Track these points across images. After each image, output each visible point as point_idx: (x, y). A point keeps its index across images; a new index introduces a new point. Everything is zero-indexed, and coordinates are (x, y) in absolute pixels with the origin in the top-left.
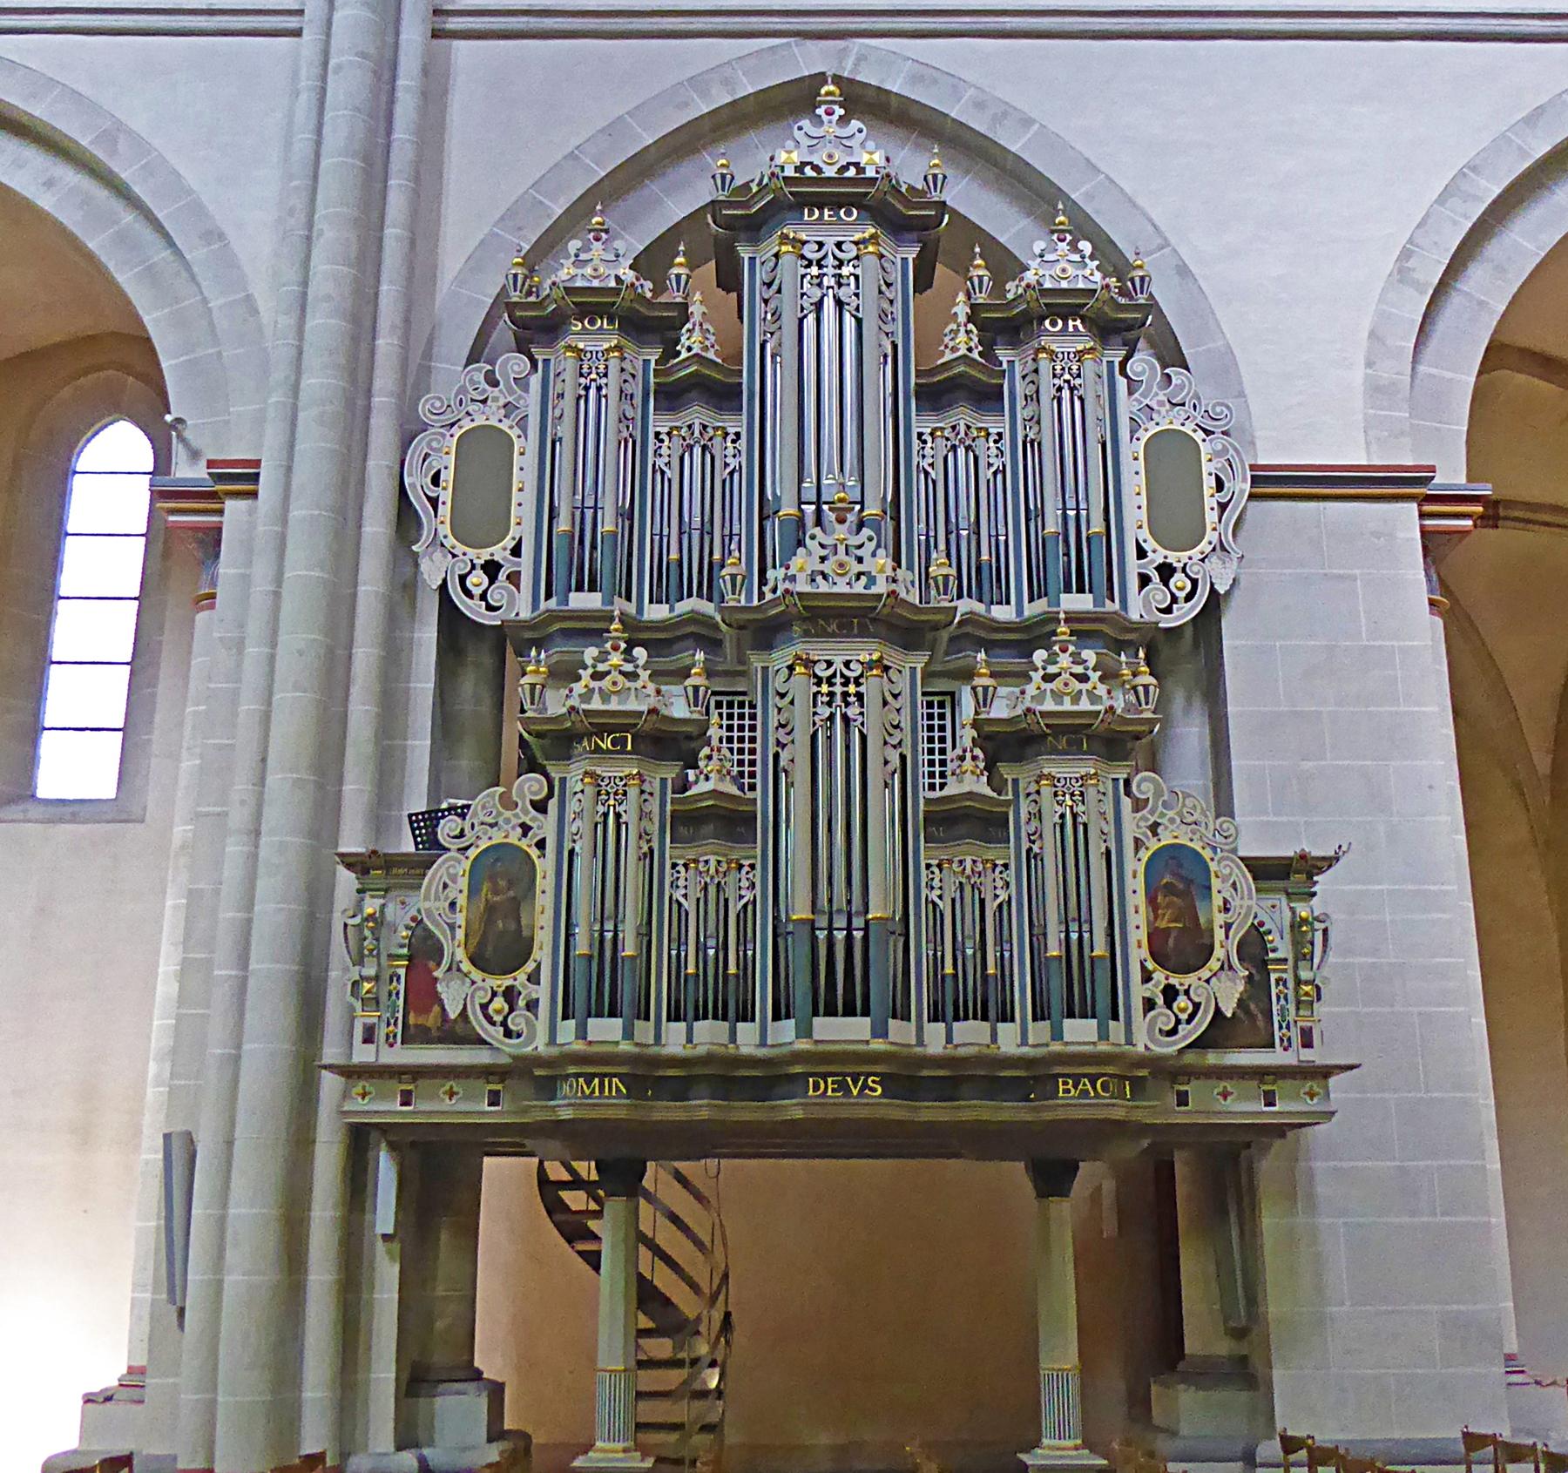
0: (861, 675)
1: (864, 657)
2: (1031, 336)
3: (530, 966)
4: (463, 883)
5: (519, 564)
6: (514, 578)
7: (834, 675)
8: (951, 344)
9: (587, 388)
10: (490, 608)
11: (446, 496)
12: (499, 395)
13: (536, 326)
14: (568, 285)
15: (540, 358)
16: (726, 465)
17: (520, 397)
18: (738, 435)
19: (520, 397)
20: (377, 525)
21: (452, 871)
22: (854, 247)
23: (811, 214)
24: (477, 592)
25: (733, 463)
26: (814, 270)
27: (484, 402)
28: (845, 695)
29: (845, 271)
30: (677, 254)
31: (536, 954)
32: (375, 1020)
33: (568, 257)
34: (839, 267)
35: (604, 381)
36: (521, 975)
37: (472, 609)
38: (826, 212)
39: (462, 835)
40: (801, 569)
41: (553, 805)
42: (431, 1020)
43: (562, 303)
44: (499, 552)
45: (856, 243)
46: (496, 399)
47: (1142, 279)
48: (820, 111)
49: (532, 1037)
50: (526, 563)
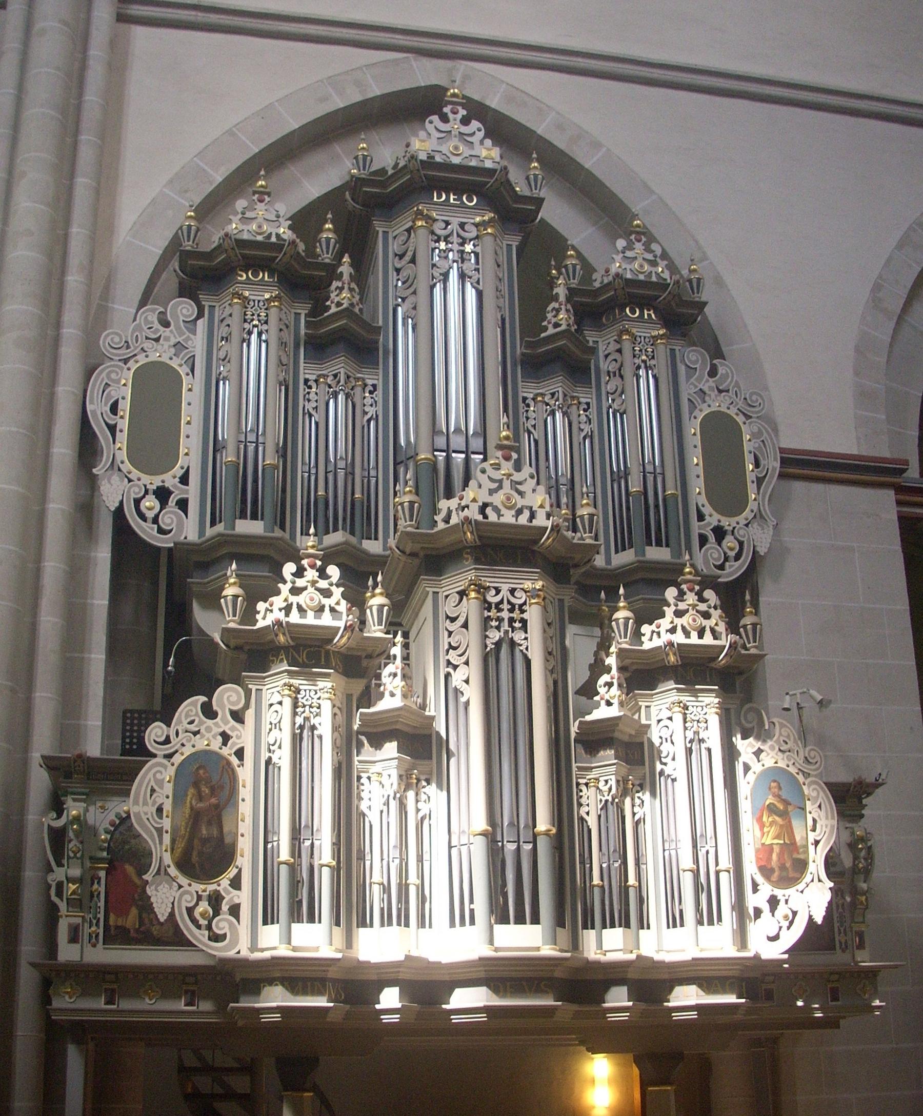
0: (525, 603)
1: (528, 585)
2: (615, 321)
3: (232, 872)
4: (169, 789)
5: (187, 492)
6: (183, 505)
7: (502, 602)
8: (554, 320)
9: (250, 333)
10: (161, 531)
11: (124, 424)
12: (171, 335)
13: (201, 272)
14: (238, 237)
15: (206, 304)
16: (366, 413)
17: (188, 339)
18: (374, 386)
19: (188, 339)
20: (63, 449)
21: (158, 776)
22: (474, 229)
23: (439, 197)
24: (150, 515)
25: (371, 411)
26: (443, 245)
27: (157, 340)
28: (512, 621)
29: (469, 248)
30: (326, 222)
31: (239, 861)
32: (79, 920)
33: (236, 213)
34: (462, 244)
35: (265, 327)
36: (224, 882)
37: (146, 531)
38: (452, 197)
39: (167, 741)
40: (474, 500)
41: (250, 715)
42: (131, 919)
43: (232, 254)
44: (170, 479)
45: (477, 225)
46: (167, 339)
47: (699, 280)
48: (447, 110)
49: (235, 941)
50: (193, 492)
